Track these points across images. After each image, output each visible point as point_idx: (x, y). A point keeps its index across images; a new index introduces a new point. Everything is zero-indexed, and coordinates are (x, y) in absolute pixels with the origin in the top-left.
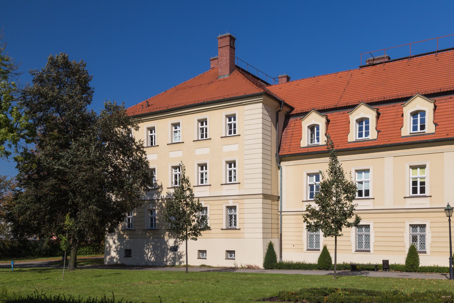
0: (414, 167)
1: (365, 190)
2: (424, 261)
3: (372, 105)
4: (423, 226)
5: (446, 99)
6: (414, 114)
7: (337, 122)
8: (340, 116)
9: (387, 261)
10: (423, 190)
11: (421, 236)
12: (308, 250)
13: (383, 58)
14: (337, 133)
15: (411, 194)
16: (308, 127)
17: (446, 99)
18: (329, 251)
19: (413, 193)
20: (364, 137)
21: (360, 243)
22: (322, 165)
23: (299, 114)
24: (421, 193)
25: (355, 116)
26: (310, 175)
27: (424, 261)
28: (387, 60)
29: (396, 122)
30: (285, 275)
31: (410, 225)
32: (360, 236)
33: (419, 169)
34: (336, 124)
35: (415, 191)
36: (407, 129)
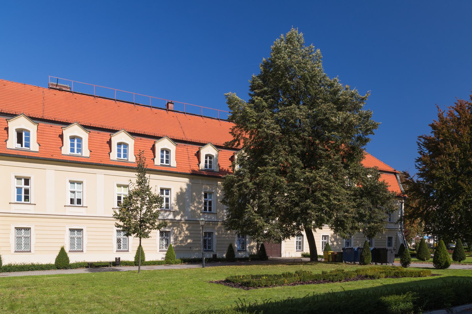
0: (119, 186)
1: (78, 199)
2: (148, 258)
3: (87, 128)
4: (80, 230)
5: (138, 139)
6: (119, 144)
7: (45, 132)
8: (47, 127)
9: (119, 258)
10: (27, 198)
11: (25, 238)
12: (16, 252)
13: (67, 87)
14: (47, 143)
15: (69, 204)
16: (16, 129)
17: (138, 139)
18: (145, 252)
19: (17, 200)
20: (75, 153)
21: (19, 245)
22: (131, 179)
23: (4, 113)
24: (77, 204)
25: (68, 132)
26: (19, 178)
27: (148, 258)
28: (69, 90)
29: (103, 147)
30: (32, 277)
31: (15, 228)
32: (19, 238)
33: (122, 187)
34: (45, 135)
35: (19, 198)
36: (66, 150)
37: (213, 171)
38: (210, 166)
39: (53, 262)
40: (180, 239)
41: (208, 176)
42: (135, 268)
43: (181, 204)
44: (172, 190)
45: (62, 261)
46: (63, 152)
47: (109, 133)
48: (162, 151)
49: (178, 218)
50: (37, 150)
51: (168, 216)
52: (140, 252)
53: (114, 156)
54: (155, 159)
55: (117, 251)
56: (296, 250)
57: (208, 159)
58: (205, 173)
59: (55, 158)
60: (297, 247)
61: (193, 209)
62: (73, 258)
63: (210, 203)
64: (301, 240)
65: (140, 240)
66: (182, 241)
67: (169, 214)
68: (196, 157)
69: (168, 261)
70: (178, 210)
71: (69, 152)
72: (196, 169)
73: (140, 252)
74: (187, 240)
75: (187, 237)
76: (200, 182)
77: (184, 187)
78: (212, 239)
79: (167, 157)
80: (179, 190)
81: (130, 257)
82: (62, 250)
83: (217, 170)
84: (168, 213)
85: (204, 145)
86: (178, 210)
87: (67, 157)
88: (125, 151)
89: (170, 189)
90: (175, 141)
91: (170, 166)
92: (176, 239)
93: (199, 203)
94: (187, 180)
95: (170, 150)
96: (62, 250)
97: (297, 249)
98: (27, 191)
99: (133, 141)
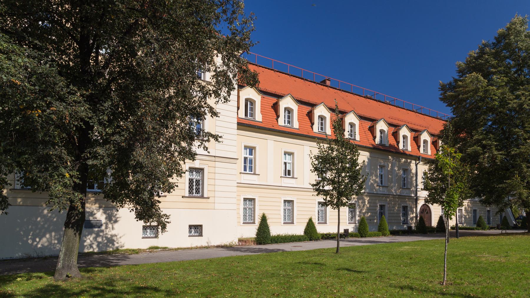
37: (384, 146)
38: (381, 141)
39: (302, 233)
40: (364, 211)
41: (384, 150)
44: (257, 149)
45: (310, 232)
46: (314, 131)
50: (261, 120)
53: (282, 121)
55: (244, 223)
58: (381, 147)
60: (319, 217)
62: (321, 229)
64: (290, 208)
68: (273, 110)
69: (362, 231)
71: (244, 117)
82: (310, 220)
88: (252, 109)
93: (376, 176)
95: (255, 101)
96: (310, 220)
97: (319, 220)
98: (251, 161)
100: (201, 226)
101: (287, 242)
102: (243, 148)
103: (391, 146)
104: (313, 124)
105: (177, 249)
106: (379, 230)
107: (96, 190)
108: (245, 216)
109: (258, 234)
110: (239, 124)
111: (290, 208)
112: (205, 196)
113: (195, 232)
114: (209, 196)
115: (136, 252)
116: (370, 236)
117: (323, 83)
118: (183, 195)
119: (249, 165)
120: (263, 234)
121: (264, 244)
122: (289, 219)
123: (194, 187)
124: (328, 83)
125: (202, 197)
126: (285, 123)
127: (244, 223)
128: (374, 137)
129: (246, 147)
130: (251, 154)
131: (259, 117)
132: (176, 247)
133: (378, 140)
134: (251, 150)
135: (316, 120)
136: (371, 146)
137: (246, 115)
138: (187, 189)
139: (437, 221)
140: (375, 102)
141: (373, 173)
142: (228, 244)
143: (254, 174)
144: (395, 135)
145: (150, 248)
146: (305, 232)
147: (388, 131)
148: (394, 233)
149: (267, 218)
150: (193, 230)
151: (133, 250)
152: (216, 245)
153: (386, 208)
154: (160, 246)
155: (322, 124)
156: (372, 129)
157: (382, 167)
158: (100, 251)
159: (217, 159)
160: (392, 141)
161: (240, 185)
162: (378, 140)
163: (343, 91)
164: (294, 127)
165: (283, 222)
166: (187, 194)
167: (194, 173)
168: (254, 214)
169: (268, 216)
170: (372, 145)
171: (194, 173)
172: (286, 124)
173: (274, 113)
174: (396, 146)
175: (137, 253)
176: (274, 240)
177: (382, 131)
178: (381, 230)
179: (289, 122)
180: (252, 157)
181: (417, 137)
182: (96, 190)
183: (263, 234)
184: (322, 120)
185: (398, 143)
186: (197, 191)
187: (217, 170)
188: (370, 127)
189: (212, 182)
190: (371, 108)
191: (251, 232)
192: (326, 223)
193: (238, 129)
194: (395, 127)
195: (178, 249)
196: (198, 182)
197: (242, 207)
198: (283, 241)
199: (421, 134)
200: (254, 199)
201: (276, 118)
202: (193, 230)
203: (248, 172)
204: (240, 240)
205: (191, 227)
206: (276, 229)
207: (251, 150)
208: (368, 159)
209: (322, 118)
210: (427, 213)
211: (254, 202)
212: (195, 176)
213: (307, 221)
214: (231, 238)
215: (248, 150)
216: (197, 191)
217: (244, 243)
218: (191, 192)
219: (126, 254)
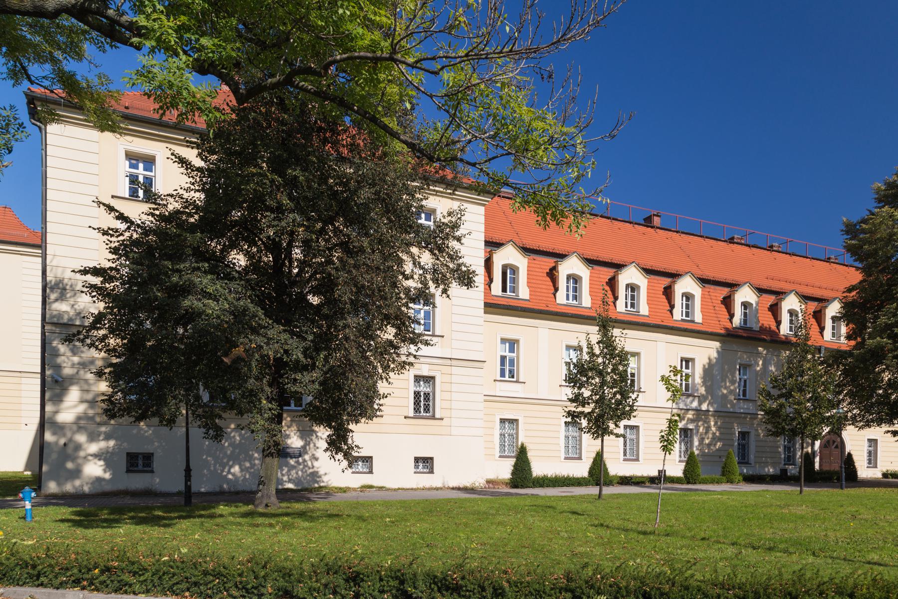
6: (569, 277)
37: (750, 330)
38: (745, 321)
39: (534, 475)
40: (707, 441)
42: (594, 490)
43: (709, 384)
46: (558, 301)
47: (555, 260)
48: (569, 277)
49: (704, 407)
50: (527, 297)
51: (691, 403)
52: (599, 461)
54: (558, 294)
56: (622, 457)
57: (571, 285)
58: (741, 333)
59: (551, 309)
61: (725, 392)
63: (745, 381)
64: (634, 437)
65: (602, 441)
66: (709, 445)
67: (693, 400)
68: (548, 279)
69: (690, 475)
70: (704, 393)
72: (728, 325)
73: (599, 461)
74: (715, 445)
75: (715, 439)
76: (735, 347)
77: (714, 355)
78: (748, 443)
79: (575, 290)
80: (706, 361)
81: (581, 469)
83: (756, 327)
84: (691, 398)
85: (562, 256)
86: (704, 393)
87: (563, 307)
89: (517, 341)
90: (526, 250)
91: (693, 321)
92: (701, 440)
93: (733, 382)
94: (717, 344)
95: (518, 268)
97: (625, 455)
98: (512, 362)
99: (646, 281)
100: (432, 459)
101: (559, 486)
102: (499, 341)
103: (764, 330)
104: (672, 307)
105: (395, 490)
106: (723, 474)
107: (293, 407)
108: (567, 447)
109: (513, 473)
110: (487, 305)
111: (634, 437)
112: (437, 416)
113: (424, 468)
114: (443, 416)
115: (344, 490)
116: (704, 482)
117: (648, 222)
118: (406, 415)
119: (508, 369)
120: (522, 474)
121: (523, 487)
122: (632, 454)
123: (422, 404)
124: (657, 221)
125: (433, 417)
126: (568, 299)
127: (500, 457)
128: (732, 316)
129: (503, 341)
130: (512, 350)
131: (524, 292)
132: (408, 487)
133: (737, 320)
134: (513, 344)
135: (678, 301)
136: (722, 332)
137: (504, 289)
138: (412, 406)
139: (856, 464)
140: (747, 248)
141: (727, 377)
142: (468, 485)
143: (517, 382)
144: (775, 310)
145: (363, 487)
146: (590, 472)
147: (757, 304)
148: (750, 479)
149: (528, 449)
150: (421, 465)
151: (340, 489)
152: (451, 486)
153: (752, 437)
154: (375, 484)
155: (687, 307)
156: (728, 302)
157: (745, 367)
158: (94, 492)
159: (454, 362)
160: (767, 320)
161: (490, 398)
162: (737, 320)
163: (683, 233)
164: (584, 305)
165: (563, 456)
166: (411, 414)
167: (422, 383)
168: (580, 445)
169: (529, 447)
170: (727, 329)
171: (422, 383)
172: (629, 308)
173: (551, 284)
174: (774, 327)
175: (345, 492)
176: (538, 482)
177: (745, 305)
178: (726, 475)
179: (575, 298)
180: (514, 355)
181: (820, 311)
182: (293, 407)
183: (522, 474)
184: (688, 299)
185: (779, 323)
186: (427, 409)
187: (454, 379)
188: (724, 298)
189: (447, 396)
190: (723, 258)
191: (504, 470)
192: (637, 460)
193: (485, 313)
194: (774, 295)
195: (399, 489)
196: (427, 395)
197: (497, 432)
198: (594, 483)
199: (826, 307)
200: (517, 420)
201: (553, 291)
202: (421, 465)
203: (507, 378)
204: (488, 482)
205: (417, 460)
206: (539, 468)
207: (513, 344)
208: (718, 352)
209: (688, 297)
210: (837, 447)
211: (517, 425)
212: (423, 388)
213: (594, 455)
214: (476, 477)
215: (507, 344)
216: (427, 409)
217: (491, 485)
218: (417, 409)
219: (329, 492)
